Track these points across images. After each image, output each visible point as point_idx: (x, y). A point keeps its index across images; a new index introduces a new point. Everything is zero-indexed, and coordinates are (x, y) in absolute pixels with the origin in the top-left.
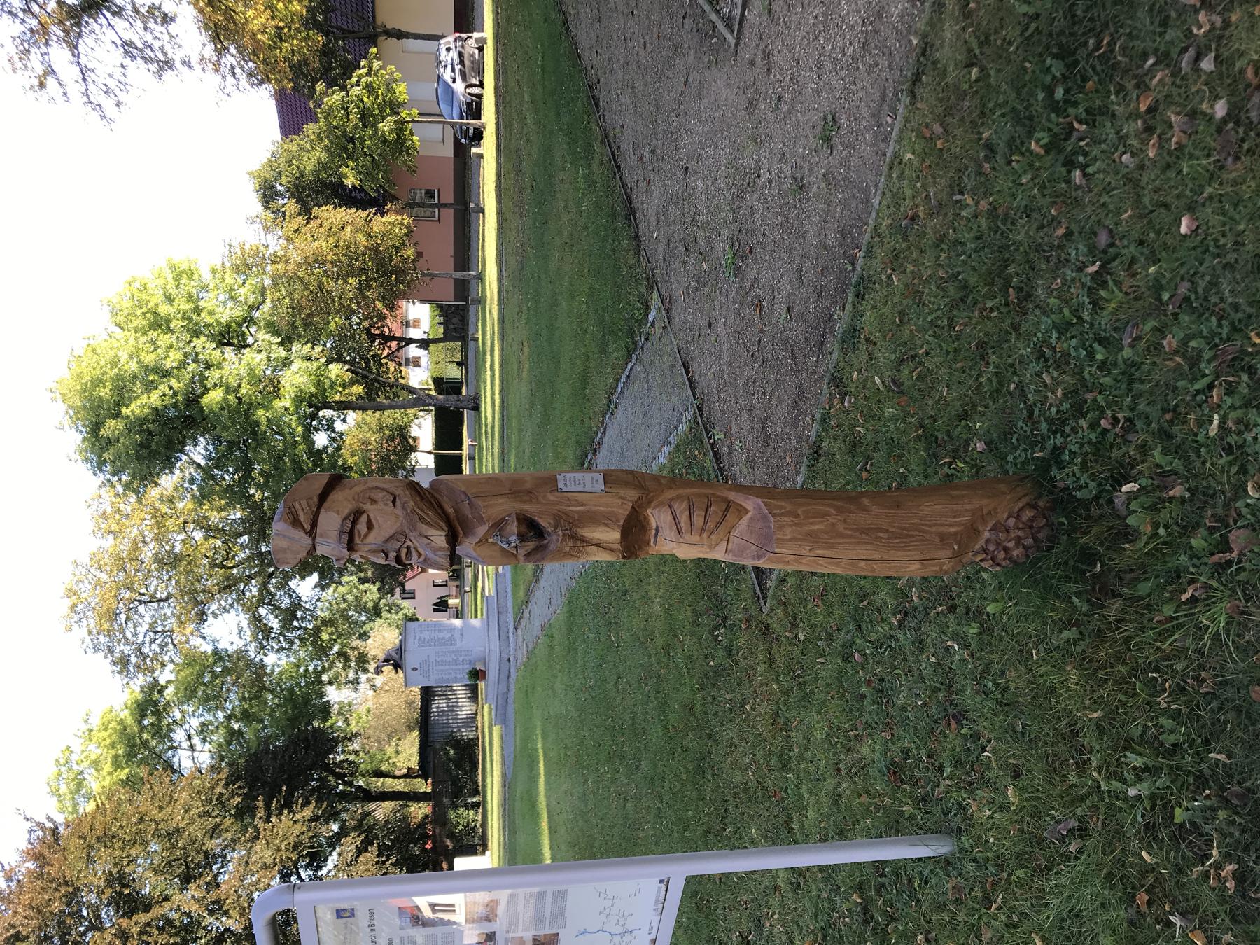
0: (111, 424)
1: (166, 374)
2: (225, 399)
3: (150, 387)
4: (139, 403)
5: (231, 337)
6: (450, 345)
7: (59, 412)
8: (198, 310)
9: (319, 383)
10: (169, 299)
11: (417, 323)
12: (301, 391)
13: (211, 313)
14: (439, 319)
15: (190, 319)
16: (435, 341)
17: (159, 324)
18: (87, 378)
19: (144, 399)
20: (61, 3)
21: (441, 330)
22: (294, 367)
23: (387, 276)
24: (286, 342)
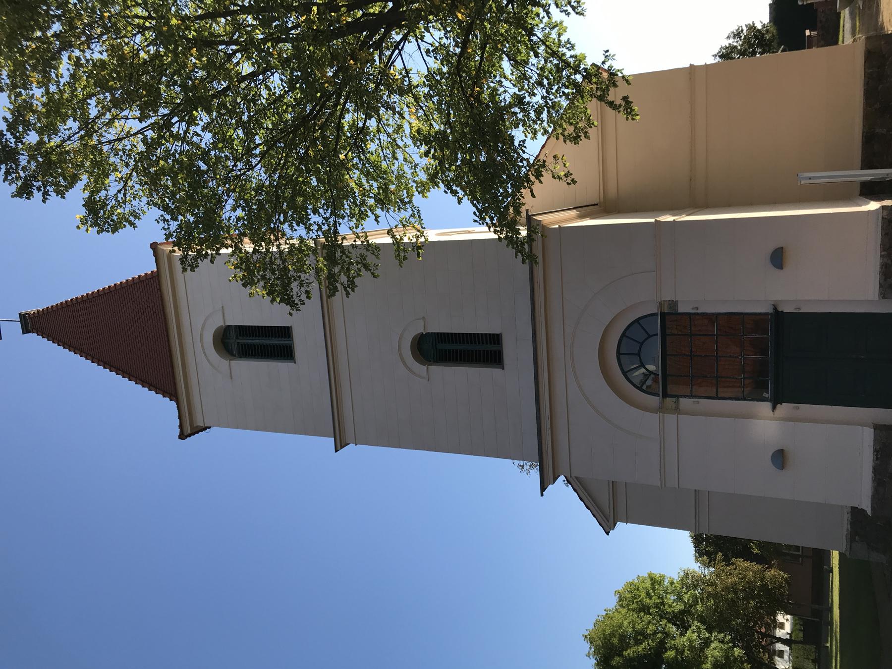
0: (617, 659)
1: (646, 636)
2: (676, 657)
3: (638, 642)
4: (632, 650)
5: (681, 620)
6: (808, 647)
7: (586, 646)
8: (663, 604)
9: (727, 658)
10: (648, 594)
11: (782, 626)
12: (717, 661)
13: (670, 606)
14: (798, 627)
15: (659, 608)
16: (796, 642)
17: (644, 609)
18: (608, 632)
19: (634, 648)
20: (160, 13)
21: (801, 635)
22: (713, 645)
23: (774, 601)
24: (710, 630)
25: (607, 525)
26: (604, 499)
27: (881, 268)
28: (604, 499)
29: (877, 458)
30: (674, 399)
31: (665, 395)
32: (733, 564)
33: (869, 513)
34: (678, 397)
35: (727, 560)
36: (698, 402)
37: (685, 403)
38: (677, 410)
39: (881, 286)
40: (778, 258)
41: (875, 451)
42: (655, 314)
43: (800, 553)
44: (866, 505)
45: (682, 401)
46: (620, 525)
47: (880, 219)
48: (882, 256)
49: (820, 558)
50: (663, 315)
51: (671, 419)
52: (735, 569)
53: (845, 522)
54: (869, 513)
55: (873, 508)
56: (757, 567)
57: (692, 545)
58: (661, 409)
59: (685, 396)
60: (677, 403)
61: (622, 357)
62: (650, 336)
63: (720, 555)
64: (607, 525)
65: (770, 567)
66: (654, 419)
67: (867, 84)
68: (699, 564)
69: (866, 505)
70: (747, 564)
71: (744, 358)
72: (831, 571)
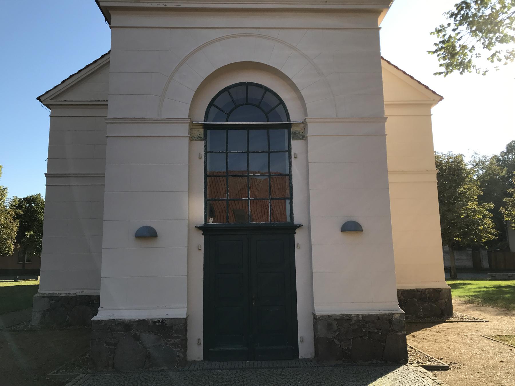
25: (47, 99)
26: (72, 97)
27: (347, 315)
28: (72, 97)
29: (155, 322)
30: (202, 136)
31: (206, 127)
32: (14, 220)
33: (95, 318)
34: (205, 139)
35: (17, 217)
36: (200, 158)
37: (200, 146)
38: (192, 138)
39: (329, 316)
40: (351, 227)
41: (163, 321)
42: (288, 118)
43: (26, 262)
44: (103, 314)
45: (201, 144)
46: (47, 112)
47: (391, 312)
48: (358, 315)
49: (34, 274)
50: (288, 126)
51: (184, 130)
52: (10, 222)
53: (67, 292)
54: (95, 318)
55: (99, 322)
56: (14, 235)
57: (26, 197)
58: (192, 125)
59: (206, 146)
60: (198, 139)
61: (213, 108)
62: (266, 115)
63: (21, 212)
64: (47, 99)
65: (15, 244)
66: (184, 114)
67: (418, 290)
68: (12, 198)
69: (103, 314)
70: (15, 229)
71: (248, 200)
72: (15, 281)
